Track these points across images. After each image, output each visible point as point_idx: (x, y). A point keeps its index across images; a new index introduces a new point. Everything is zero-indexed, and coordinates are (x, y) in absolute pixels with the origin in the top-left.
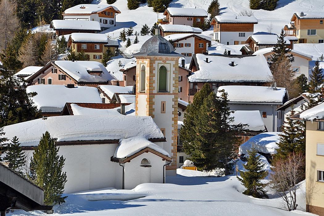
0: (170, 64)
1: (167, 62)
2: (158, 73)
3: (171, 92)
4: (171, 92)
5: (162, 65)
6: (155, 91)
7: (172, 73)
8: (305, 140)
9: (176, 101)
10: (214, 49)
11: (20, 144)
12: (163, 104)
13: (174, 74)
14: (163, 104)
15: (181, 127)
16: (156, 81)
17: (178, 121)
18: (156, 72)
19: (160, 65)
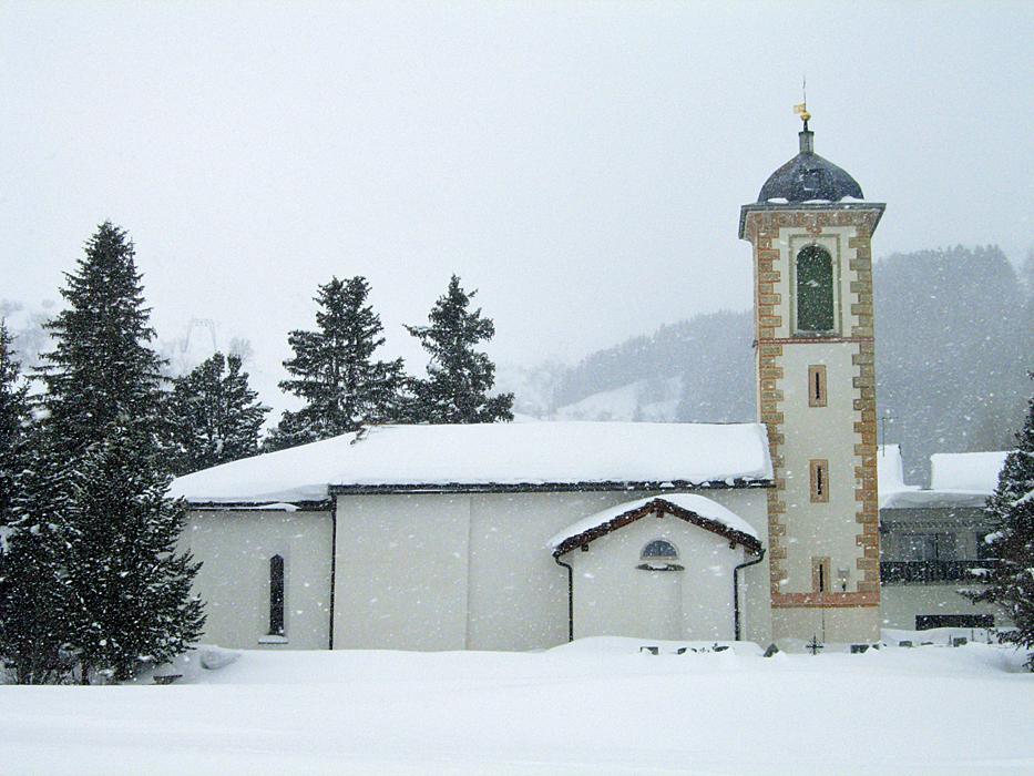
0: (837, 237)
1: (825, 230)
2: (791, 269)
3: (847, 333)
4: (847, 333)
5: (807, 242)
6: (782, 332)
7: (845, 266)
8: (253, 454)
9: (865, 364)
10: (915, 549)
11: (200, 565)
12: (817, 375)
13: (855, 272)
14: (817, 375)
15: (18, 308)
16: (786, 297)
17: (936, 458)
18: (784, 267)
19: (799, 245)
